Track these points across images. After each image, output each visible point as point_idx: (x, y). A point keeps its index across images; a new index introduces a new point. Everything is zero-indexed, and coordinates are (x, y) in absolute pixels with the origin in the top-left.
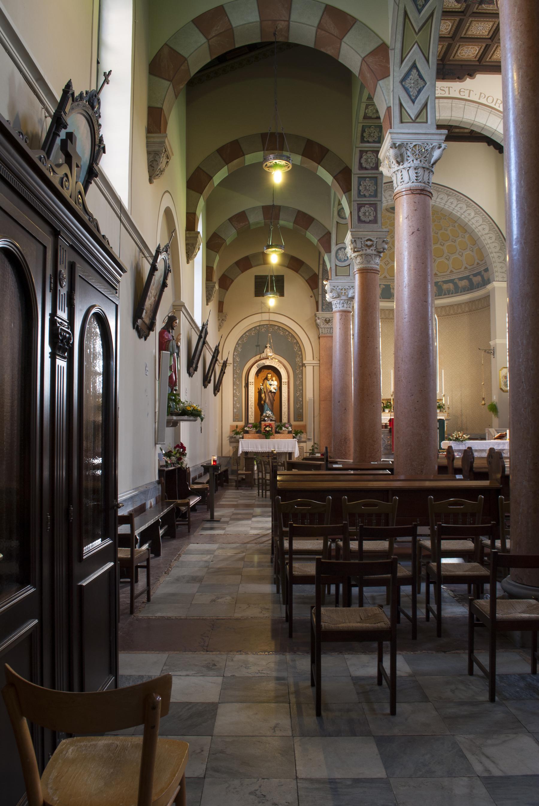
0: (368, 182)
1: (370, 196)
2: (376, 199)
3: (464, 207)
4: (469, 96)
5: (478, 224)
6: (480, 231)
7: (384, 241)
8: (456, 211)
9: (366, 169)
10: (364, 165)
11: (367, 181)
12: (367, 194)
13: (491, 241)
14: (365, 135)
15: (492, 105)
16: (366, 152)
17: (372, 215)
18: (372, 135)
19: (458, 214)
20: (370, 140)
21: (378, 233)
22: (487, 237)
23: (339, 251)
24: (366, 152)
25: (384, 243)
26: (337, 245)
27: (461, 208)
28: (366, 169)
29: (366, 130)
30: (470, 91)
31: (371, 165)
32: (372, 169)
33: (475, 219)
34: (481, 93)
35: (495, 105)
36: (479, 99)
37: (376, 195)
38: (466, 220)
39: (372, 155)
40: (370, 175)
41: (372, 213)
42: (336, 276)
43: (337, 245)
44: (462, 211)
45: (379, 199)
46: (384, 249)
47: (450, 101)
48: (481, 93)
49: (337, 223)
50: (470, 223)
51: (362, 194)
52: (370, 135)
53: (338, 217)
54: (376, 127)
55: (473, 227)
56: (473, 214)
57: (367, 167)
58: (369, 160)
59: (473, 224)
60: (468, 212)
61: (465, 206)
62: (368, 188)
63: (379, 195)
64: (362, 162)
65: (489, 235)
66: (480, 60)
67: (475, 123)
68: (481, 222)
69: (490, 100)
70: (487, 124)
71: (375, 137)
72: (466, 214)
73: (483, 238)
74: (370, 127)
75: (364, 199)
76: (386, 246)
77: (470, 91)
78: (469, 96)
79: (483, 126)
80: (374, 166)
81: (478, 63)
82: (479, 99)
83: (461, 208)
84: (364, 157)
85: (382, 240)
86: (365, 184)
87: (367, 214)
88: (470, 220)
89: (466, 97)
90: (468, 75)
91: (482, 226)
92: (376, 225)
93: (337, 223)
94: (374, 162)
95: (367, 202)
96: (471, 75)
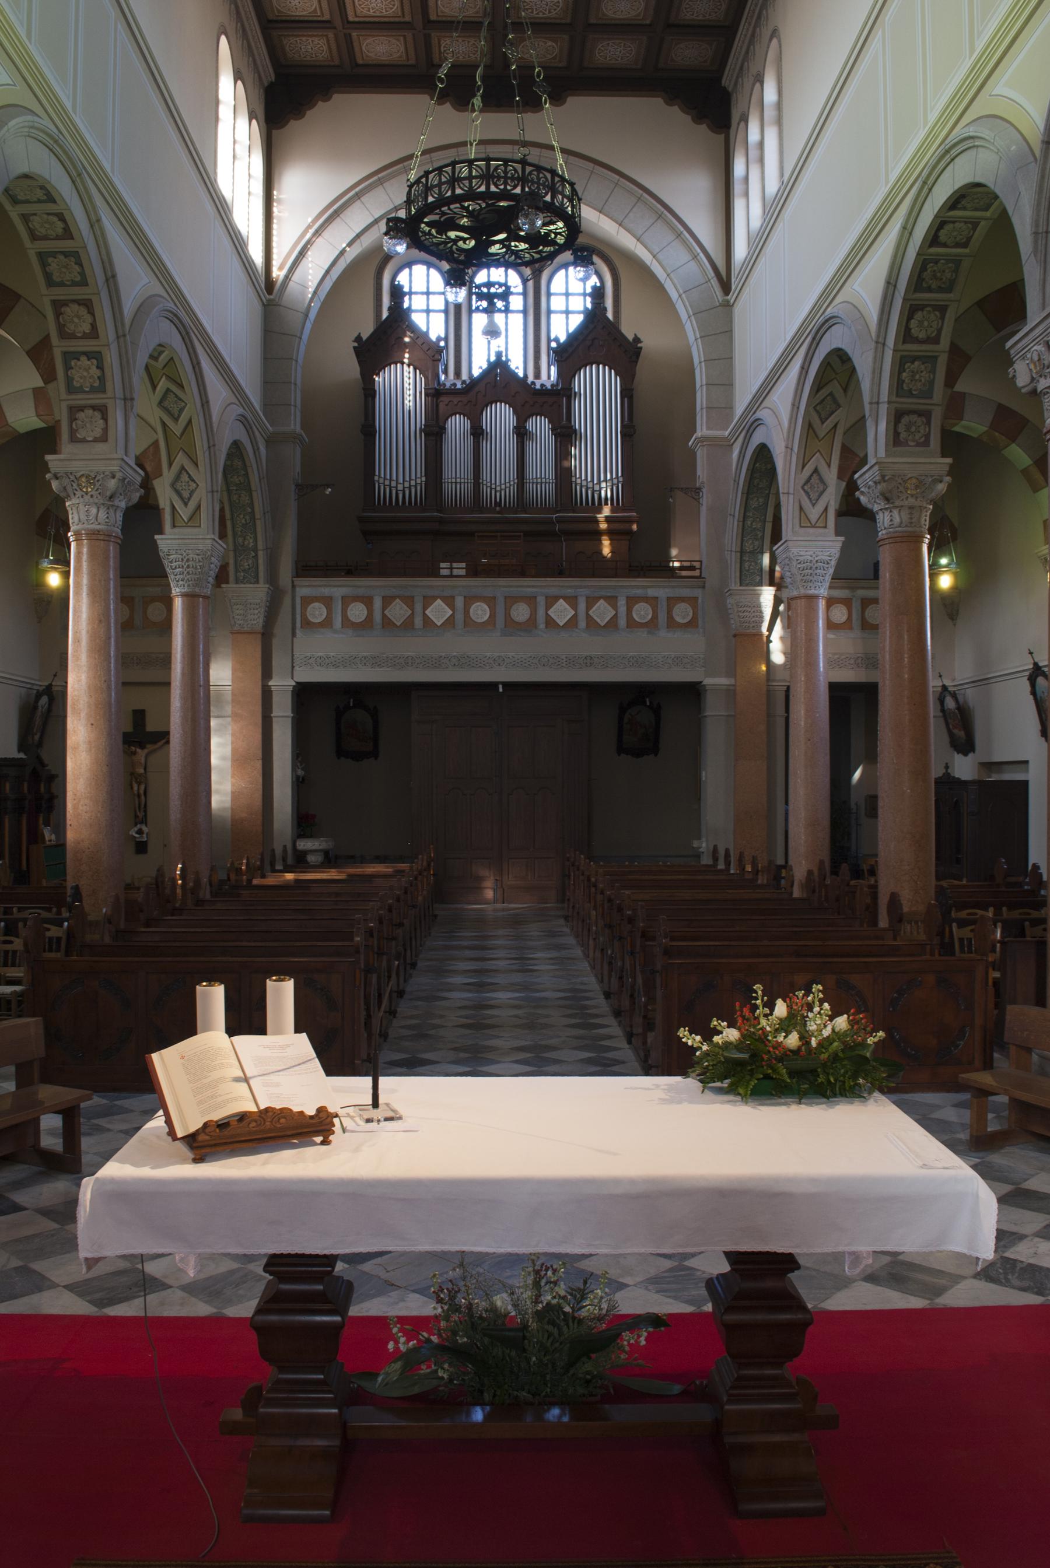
11: (88, 385)
42: (174, 526)
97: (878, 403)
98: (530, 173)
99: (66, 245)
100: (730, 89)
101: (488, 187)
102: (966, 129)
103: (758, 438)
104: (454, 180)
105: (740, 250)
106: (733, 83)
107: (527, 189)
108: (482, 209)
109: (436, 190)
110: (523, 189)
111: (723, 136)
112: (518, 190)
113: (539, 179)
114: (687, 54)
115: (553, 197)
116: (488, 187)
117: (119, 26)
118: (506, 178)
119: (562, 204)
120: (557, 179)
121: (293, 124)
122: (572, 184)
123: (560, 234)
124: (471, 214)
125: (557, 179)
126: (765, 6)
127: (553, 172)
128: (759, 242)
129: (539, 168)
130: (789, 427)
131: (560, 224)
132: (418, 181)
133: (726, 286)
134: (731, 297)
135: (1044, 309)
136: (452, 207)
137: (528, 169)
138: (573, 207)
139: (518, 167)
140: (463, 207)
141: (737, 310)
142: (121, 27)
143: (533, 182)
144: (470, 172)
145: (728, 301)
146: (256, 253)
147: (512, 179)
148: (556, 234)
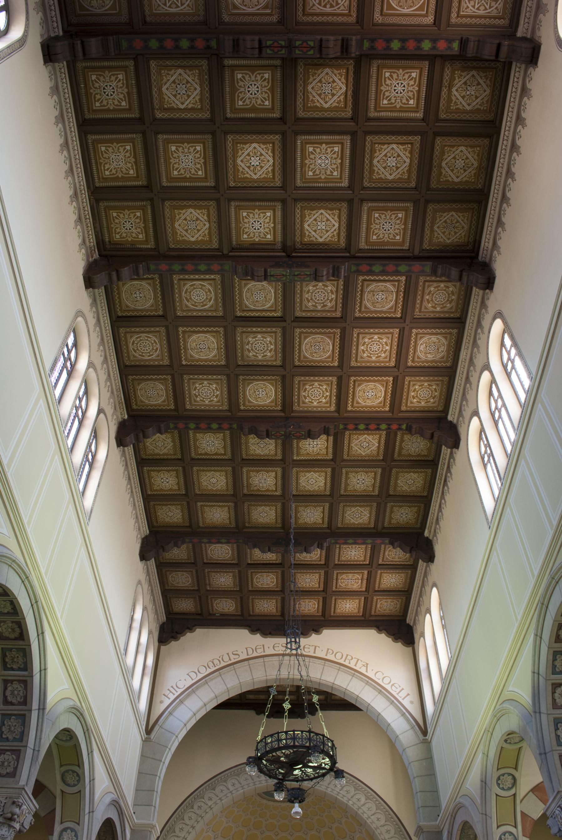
0: (13, 722)
1: (15, 740)
2: (20, 744)
3: (352, 790)
4: (314, 653)
5: (370, 813)
6: (373, 822)
7: (14, 803)
8: (341, 795)
9: (12, 704)
10: (10, 699)
11: (12, 720)
12: (11, 737)
13: (390, 836)
14: (7, 660)
15: (342, 661)
16: (12, 681)
17: (12, 766)
18: (15, 660)
19: (345, 800)
20: (15, 666)
21: (9, 790)
22: (383, 829)
23: (64, 833)
24: (12, 681)
25: (15, 805)
26: (61, 823)
27: (347, 792)
28: (12, 704)
29: (7, 654)
30: (316, 647)
31: (19, 699)
32: (20, 704)
33: (367, 806)
34: (328, 649)
35: (345, 661)
36: (326, 655)
37: (21, 740)
38: (355, 808)
39: (19, 686)
40: (16, 712)
41: (13, 763)
43: (61, 823)
44: (349, 796)
45: (24, 744)
46: (13, 814)
47: (261, 660)
48: (328, 649)
49: (62, 791)
50: (360, 812)
51: (4, 736)
52: (13, 661)
53: (62, 784)
54: (18, 650)
55: (365, 816)
56: (363, 800)
57: (13, 701)
58: (16, 692)
59: (364, 812)
60: (357, 796)
61: (353, 789)
62: (13, 729)
63: (25, 738)
64: (7, 695)
65: (386, 828)
66: (324, 614)
67: (322, 682)
68: (374, 809)
69: (339, 656)
70: (336, 683)
71: (20, 662)
72: (354, 800)
73: (379, 831)
74: (11, 650)
75: (7, 744)
76: (17, 810)
77: (316, 647)
78: (314, 653)
79: (331, 685)
80: (22, 700)
81: (323, 618)
82: (326, 655)
83: (347, 792)
84: (10, 688)
85: (11, 801)
86: (10, 723)
87: (6, 764)
88: (359, 808)
89: (311, 654)
90: (313, 630)
91: (376, 816)
92: (12, 779)
93: (62, 791)
94: (21, 694)
95: (8, 748)
96: (317, 630)
97: (545, 753)
98: (313, 736)
99: (76, 768)
100: (411, 624)
101: (294, 743)
102: (501, 706)
103: (460, 819)
104: (279, 740)
105: (430, 707)
106: (412, 621)
107: (312, 744)
108: (291, 753)
109: (270, 745)
110: (310, 744)
111: (411, 648)
112: (308, 744)
113: (317, 739)
114: (403, 515)
115: (324, 747)
116: (294, 743)
117: (82, 549)
118: (302, 739)
119: (328, 750)
120: (325, 739)
121: (173, 643)
122: (332, 741)
123: (327, 764)
124: (286, 756)
125: (325, 739)
126: (540, 8)
127: (323, 736)
128: (440, 704)
129: (317, 734)
130: (482, 803)
131: (328, 760)
132: (261, 740)
133: (425, 732)
134: (429, 737)
135: (554, 791)
136: (277, 753)
137: (312, 734)
138: (333, 752)
139: (308, 734)
140: (282, 753)
141: (434, 743)
142: (83, 549)
143: (314, 741)
144: (286, 736)
145: (427, 739)
146: (143, 705)
147: (305, 739)
148: (325, 764)
